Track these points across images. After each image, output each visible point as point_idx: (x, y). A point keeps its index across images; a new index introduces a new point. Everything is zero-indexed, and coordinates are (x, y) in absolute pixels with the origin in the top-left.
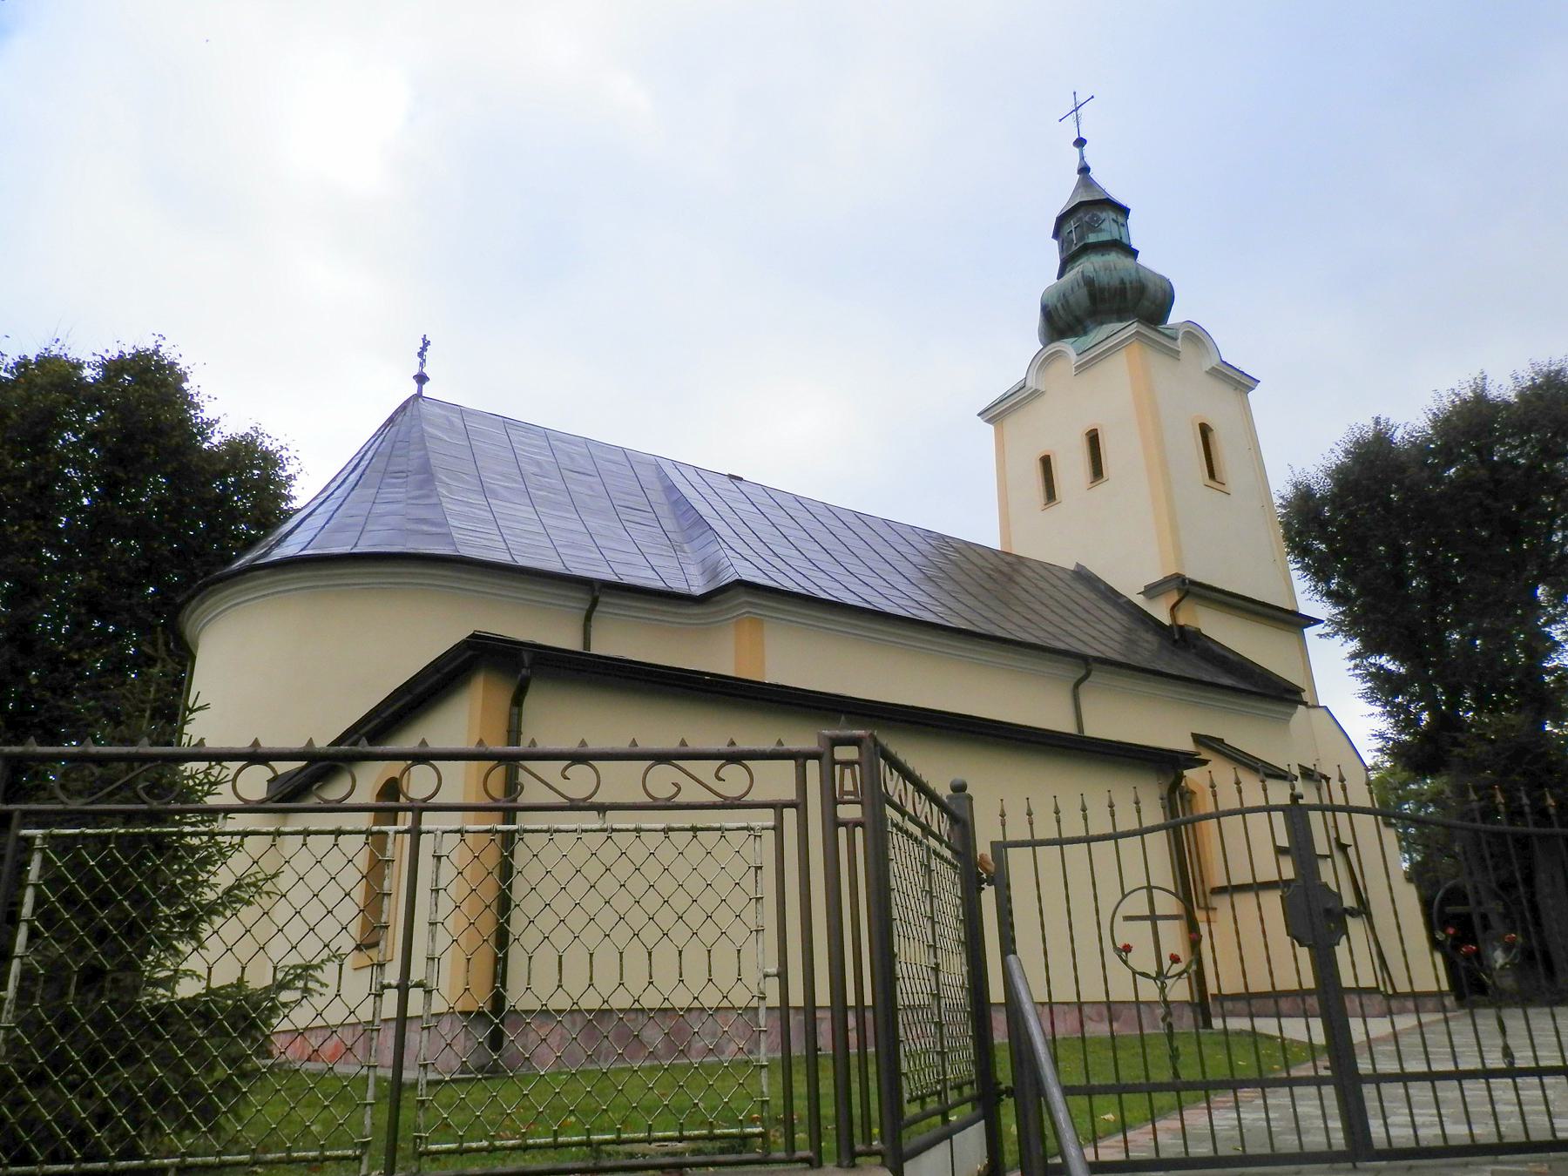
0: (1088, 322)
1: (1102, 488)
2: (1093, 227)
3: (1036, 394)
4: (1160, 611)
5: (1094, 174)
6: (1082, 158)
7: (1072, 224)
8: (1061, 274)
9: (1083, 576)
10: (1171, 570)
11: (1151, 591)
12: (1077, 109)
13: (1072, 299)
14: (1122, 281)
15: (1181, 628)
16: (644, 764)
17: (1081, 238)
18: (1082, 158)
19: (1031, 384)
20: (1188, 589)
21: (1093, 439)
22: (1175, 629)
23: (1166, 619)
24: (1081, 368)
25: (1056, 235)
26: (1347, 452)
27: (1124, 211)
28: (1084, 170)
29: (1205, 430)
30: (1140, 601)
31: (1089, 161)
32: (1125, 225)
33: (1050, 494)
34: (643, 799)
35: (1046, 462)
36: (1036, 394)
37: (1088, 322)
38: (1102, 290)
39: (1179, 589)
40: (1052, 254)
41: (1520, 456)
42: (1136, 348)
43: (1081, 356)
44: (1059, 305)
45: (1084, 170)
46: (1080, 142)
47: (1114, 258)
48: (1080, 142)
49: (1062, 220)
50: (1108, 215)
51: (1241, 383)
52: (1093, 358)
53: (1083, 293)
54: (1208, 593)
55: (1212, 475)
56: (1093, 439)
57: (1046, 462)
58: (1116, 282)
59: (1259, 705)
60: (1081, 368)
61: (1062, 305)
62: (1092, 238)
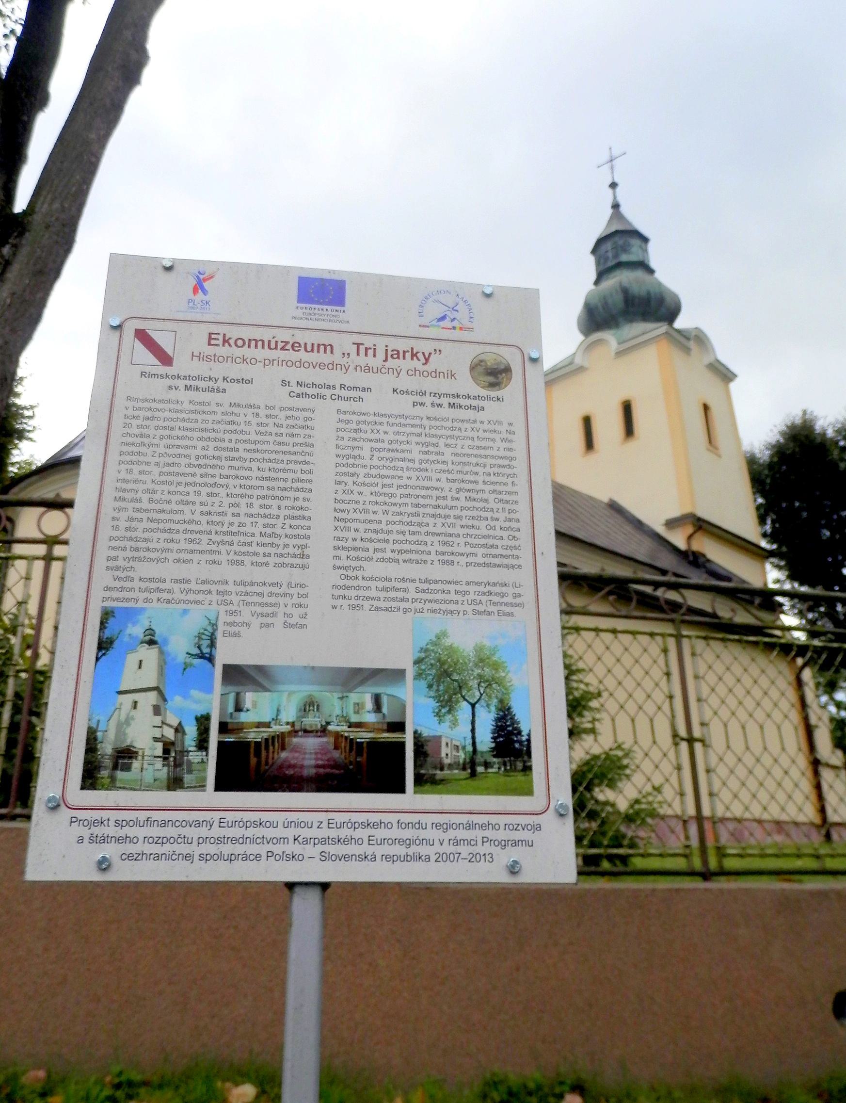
0: (621, 319)
1: (632, 444)
2: (625, 249)
3: (581, 369)
4: (679, 539)
5: (624, 209)
6: (615, 197)
7: (608, 246)
8: (597, 283)
9: (614, 507)
10: (687, 510)
11: (671, 524)
12: (611, 161)
13: (610, 301)
14: (649, 293)
15: (694, 553)
16: (41, 510)
17: (616, 256)
18: (615, 197)
19: (578, 361)
20: (701, 525)
21: (627, 409)
22: (690, 554)
23: (682, 545)
24: (619, 354)
25: (594, 251)
26: (787, 426)
27: (645, 240)
28: (616, 206)
29: (706, 408)
30: (661, 530)
31: (621, 200)
32: (645, 251)
33: (589, 444)
34: (38, 536)
35: (587, 422)
36: (581, 369)
37: (621, 319)
38: (634, 297)
39: (694, 525)
40: (589, 268)
41: (50, 204)
42: (664, 344)
43: (622, 345)
44: (599, 304)
45: (616, 206)
46: (613, 185)
47: (639, 274)
48: (613, 185)
49: (600, 242)
50: (635, 242)
51: (725, 375)
52: (629, 348)
53: (619, 299)
54: (715, 530)
55: (710, 442)
56: (627, 409)
57: (587, 422)
58: (643, 293)
59: (586, 554)
60: (619, 354)
61: (603, 307)
62: (624, 258)
